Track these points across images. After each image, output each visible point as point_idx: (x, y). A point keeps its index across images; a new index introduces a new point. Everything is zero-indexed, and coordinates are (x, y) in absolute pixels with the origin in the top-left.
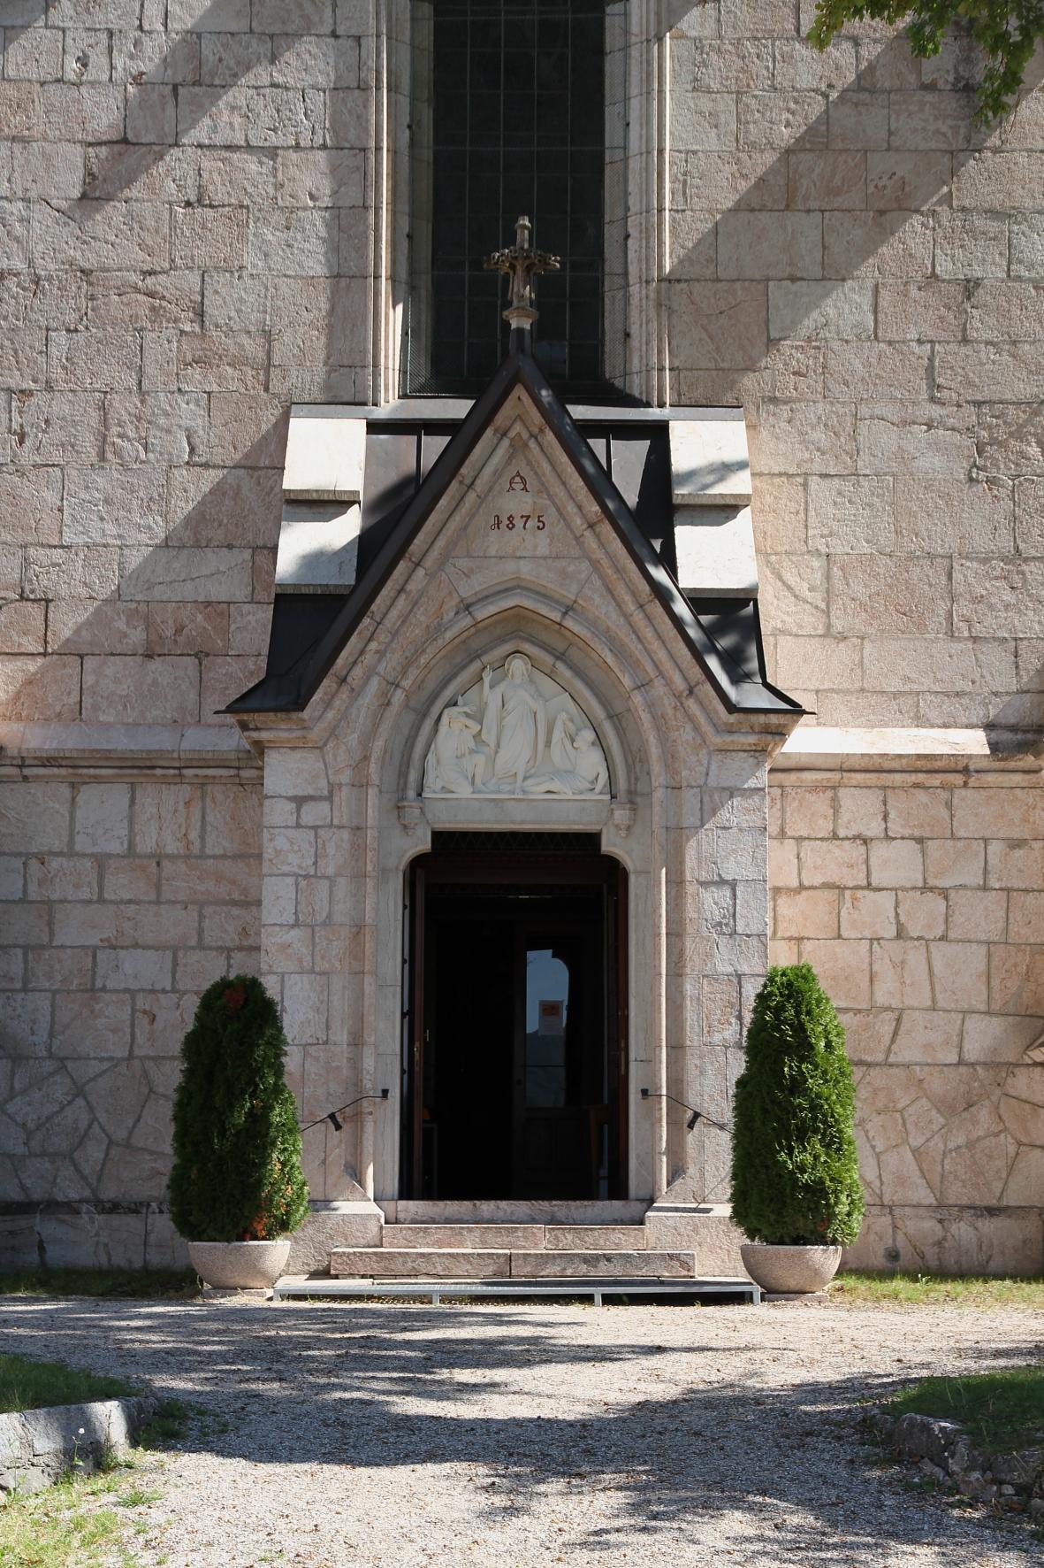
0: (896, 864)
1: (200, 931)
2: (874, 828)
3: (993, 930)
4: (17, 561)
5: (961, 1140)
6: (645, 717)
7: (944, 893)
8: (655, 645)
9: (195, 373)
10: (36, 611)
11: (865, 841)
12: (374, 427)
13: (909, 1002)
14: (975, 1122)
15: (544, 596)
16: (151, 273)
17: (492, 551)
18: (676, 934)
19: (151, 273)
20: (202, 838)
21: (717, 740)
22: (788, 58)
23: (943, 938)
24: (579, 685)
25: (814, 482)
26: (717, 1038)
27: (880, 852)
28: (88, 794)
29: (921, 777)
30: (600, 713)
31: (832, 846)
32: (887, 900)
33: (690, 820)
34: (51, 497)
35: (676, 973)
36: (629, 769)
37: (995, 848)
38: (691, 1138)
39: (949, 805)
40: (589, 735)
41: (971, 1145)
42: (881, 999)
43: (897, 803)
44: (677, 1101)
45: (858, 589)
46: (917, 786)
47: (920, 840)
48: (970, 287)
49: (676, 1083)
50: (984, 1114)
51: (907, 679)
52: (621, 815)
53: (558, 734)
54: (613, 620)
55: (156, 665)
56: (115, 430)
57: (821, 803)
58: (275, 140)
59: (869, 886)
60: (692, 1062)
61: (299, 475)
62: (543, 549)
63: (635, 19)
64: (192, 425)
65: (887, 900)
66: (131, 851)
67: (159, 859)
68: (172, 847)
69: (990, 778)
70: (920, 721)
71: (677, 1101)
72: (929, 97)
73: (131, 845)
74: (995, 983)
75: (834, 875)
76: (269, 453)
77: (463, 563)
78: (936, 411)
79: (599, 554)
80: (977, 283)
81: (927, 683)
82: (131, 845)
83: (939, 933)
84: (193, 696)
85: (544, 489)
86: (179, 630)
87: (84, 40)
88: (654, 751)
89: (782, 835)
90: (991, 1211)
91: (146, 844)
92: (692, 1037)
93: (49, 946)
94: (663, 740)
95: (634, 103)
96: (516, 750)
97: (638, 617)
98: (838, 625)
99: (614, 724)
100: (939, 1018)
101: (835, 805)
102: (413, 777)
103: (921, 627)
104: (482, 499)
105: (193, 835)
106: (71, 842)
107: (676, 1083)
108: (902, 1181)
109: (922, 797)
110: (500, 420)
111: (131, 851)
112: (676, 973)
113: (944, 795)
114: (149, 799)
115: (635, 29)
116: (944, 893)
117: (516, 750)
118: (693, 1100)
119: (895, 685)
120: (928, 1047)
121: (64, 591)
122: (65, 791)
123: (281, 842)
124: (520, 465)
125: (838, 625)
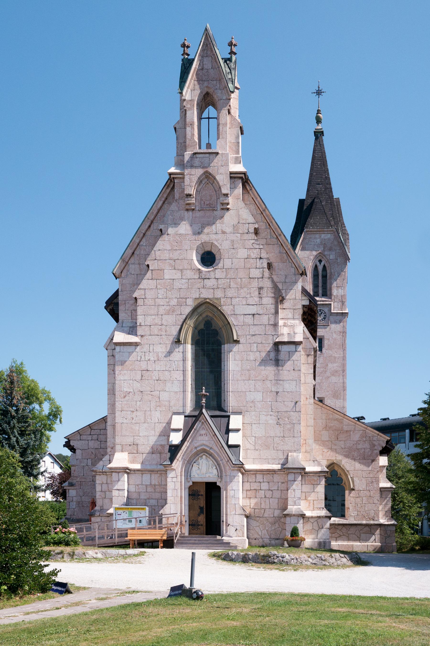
0: (265, 486)
1: (161, 497)
2: (261, 480)
3: (279, 496)
4: (132, 439)
5: (273, 528)
6: (222, 465)
7: (272, 491)
8: (223, 454)
9: (159, 408)
10: (135, 446)
11: (260, 482)
12: (185, 416)
13: (267, 507)
14: (275, 526)
15: (207, 446)
16: (152, 391)
17: (199, 439)
18: (226, 498)
19: (152, 391)
20: (161, 482)
21: (232, 469)
22: (249, 355)
23: (272, 498)
24: (189, 470)
25: (253, 425)
26: (232, 513)
27: (262, 484)
28: (144, 475)
29: (268, 472)
30: (216, 464)
31: (255, 483)
32: (263, 492)
33: (228, 481)
34: (137, 428)
35: (226, 504)
36: (220, 472)
37: (280, 483)
38: (228, 528)
39: (273, 477)
40: (215, 467)
41: (275, 529)
42: (262, 507)
43: (265, 476)
44: (226, 523)
45: (259, 442)
46: (268, 474)
47: (268, 482)
48: (277, 393)
49: (226, 520)
50: (277, 524)
51: (267, 457)
52: (219, 480)
53: (210, 467)
54: (217, 450)
55: (154, 455)
56: (147, 417)
57: (253, 476)
58: (170, 369)
59: (261, 490)
60: (228, 517)
61: (173, 426)
62: (207, 439)
63: (226, 348)
64: (158, 417)
65: (263, 492)
66: (151, 484)
67: (155, 485)
68: (157, 483)
69: (278, 472)
70: (269, 463)
71: (226, 523)
72: (271, 361)
73: (151, 483)
74: (279, 505)
75: (255, 488)
76: (169, 423)
77: (195, 441)
78: (272, 413)
79: (215, 440)
80: (278, 392)
81: (270, 457)
82: (151, 483)
83: (271, 497)
84: (159, 460)
85: (207, 430)
86: (157, 450)
87: (141, 354)
88: (223, 470)
89: (248, 481)
90: (277, 539)
91: (153, 483)
92: (229, 513)
93: (139, 499)
94: (225, 468)
95: (226, 362)
96: (204, 469)
97: (220, 450)
98: (256, 448)
99: (218, 465)
100: (271, 510)
101: (256, 477)
102: (189, 474)
103: (269, 448)
104: (198, 431)
105: (160, 482)
106: (142, 483)
107: (226, 520)
108: (265, 535)
109: (269, 475)
110: (200, 419)
111: (151, 484)
112: (226, 504)
113: (272, 475)
114: (153, 476)
115: (226, 350)
116: (272, 491)
117: (204, 469)
118: (228, 523)
119: (265, 457)
120: (269, 514)
121: (140, 443)
122: (141, 475)
123: (170, 484)
124: (203, 426)
125: (256, 448)
